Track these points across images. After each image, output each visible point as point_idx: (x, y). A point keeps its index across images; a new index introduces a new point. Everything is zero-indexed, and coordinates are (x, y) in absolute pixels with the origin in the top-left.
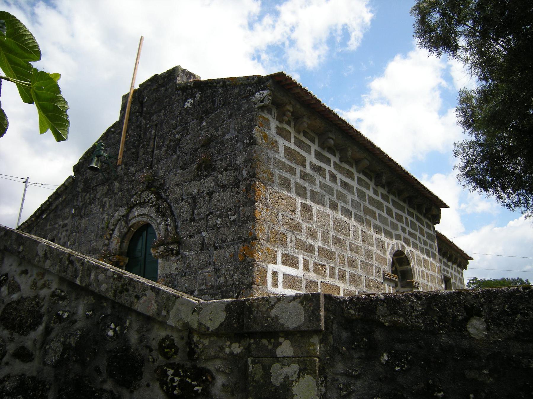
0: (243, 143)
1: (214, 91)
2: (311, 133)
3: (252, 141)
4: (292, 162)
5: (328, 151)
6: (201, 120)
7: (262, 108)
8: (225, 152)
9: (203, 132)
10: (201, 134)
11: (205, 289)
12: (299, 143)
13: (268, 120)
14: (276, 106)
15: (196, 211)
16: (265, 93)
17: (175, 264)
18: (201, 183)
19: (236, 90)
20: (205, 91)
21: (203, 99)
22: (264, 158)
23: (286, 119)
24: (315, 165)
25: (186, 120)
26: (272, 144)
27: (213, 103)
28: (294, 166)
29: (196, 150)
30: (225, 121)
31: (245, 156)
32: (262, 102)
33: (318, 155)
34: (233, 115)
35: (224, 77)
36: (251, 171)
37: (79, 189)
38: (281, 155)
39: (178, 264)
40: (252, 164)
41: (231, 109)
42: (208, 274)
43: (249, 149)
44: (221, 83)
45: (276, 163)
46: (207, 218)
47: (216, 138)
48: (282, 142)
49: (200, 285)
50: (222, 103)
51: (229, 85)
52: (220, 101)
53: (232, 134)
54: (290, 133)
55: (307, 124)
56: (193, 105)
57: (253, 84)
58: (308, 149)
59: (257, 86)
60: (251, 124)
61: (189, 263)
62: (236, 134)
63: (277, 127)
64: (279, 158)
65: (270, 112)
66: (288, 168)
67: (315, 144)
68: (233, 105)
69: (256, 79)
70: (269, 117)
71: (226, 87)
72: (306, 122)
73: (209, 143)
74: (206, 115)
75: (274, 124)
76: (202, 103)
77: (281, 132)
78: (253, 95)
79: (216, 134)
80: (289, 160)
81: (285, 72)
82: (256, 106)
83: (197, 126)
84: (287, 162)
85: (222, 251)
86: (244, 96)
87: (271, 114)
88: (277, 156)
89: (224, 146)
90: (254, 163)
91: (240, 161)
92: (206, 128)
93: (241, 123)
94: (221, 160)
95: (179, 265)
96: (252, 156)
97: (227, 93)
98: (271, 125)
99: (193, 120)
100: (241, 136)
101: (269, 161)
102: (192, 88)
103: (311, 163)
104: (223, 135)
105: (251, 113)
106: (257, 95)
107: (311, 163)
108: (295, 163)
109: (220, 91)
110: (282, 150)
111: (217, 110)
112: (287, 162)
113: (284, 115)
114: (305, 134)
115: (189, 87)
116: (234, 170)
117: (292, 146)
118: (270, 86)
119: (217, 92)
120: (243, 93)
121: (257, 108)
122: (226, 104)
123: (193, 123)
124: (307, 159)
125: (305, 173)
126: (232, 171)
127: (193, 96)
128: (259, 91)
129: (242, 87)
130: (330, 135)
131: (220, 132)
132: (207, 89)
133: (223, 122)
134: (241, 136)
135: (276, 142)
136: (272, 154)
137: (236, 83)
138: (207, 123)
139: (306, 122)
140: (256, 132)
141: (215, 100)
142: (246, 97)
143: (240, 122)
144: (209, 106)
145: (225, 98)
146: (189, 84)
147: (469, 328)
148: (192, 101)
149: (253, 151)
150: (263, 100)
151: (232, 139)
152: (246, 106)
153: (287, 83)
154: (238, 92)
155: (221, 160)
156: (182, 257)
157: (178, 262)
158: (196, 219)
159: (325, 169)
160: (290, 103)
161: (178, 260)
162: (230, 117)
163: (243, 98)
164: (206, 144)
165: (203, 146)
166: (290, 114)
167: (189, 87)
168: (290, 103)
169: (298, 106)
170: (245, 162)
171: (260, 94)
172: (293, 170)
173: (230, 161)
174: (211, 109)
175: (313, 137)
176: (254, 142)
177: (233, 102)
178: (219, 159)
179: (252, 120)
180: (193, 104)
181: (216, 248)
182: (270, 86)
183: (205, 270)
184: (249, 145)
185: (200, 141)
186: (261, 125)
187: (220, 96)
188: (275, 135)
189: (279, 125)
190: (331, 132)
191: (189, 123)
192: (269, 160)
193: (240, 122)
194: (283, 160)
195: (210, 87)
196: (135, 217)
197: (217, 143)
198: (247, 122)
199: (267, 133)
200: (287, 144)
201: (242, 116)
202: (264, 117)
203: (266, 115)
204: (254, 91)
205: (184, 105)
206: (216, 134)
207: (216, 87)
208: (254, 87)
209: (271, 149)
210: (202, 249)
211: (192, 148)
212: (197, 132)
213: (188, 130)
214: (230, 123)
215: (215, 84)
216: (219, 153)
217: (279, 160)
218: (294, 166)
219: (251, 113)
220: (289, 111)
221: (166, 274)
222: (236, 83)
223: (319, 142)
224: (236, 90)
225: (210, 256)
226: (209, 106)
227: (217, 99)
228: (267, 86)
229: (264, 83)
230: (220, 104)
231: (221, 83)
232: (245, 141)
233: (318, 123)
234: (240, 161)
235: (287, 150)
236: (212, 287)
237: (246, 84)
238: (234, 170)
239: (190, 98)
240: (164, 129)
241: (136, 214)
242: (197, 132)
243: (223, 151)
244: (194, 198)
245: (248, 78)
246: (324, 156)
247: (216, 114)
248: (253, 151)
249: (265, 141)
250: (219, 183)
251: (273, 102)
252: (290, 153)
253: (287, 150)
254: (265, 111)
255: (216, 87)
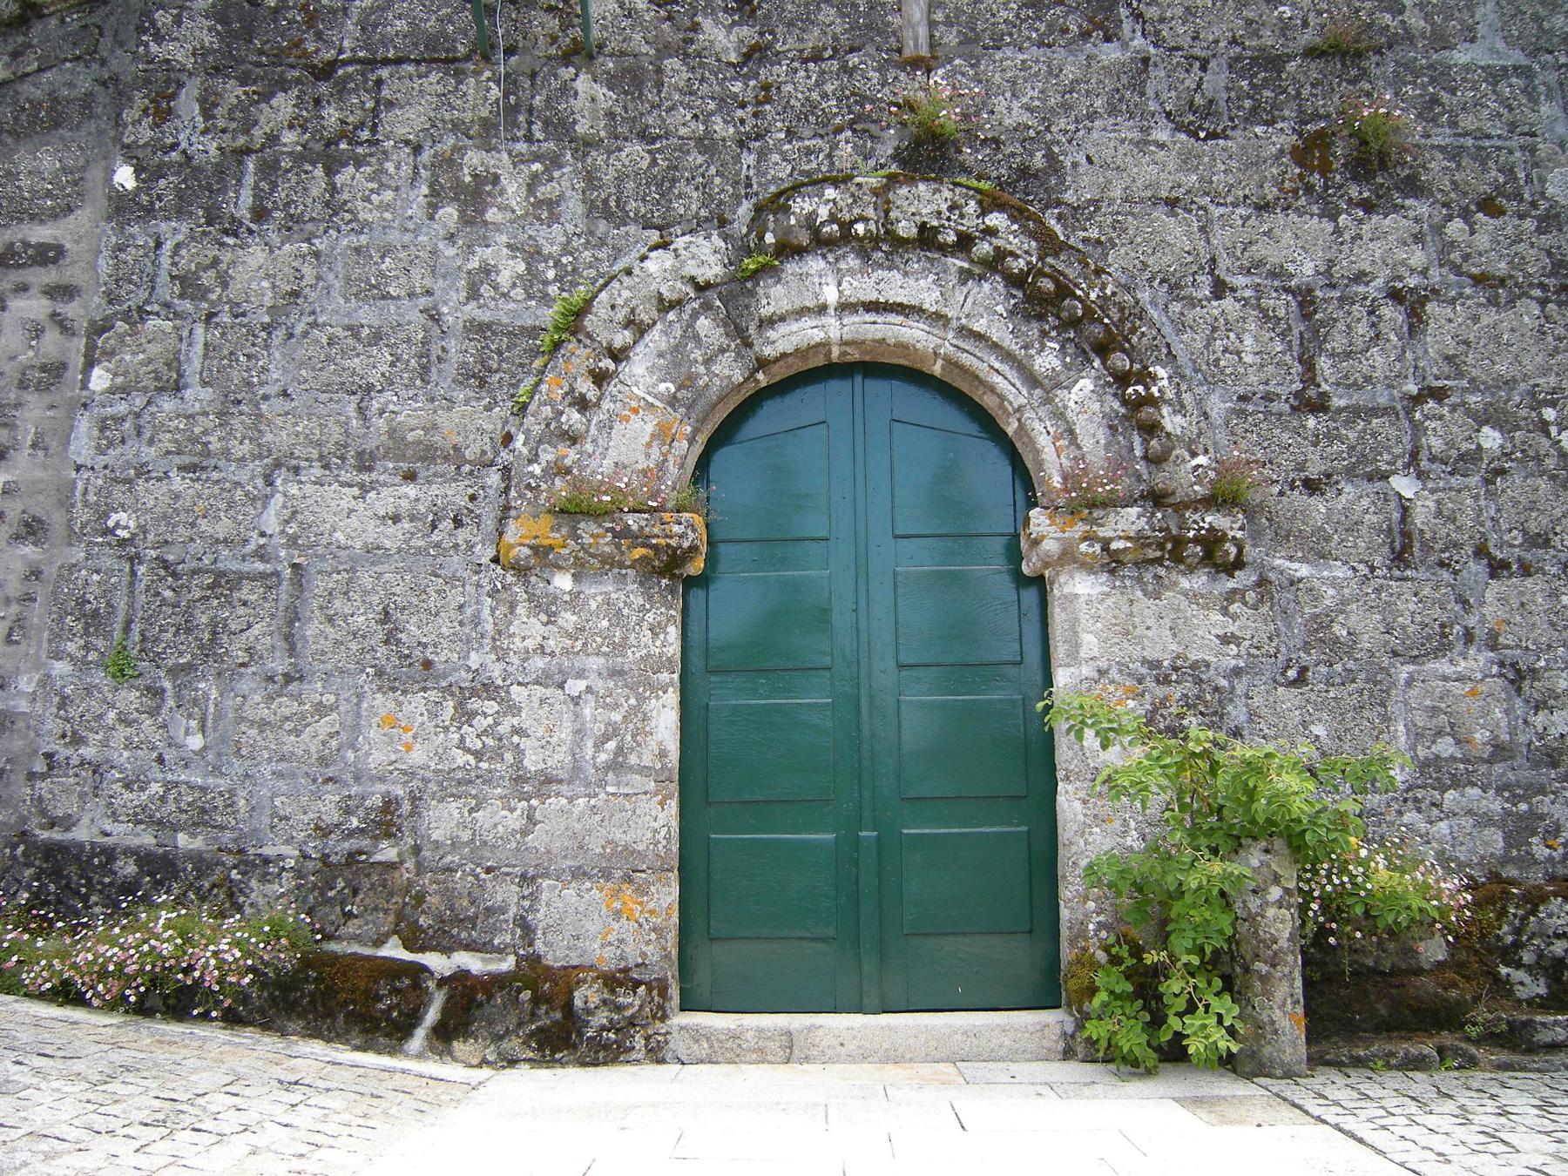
11: (1453, 758)
15: (1323, 363)
17: (1216, 617)
18: (1338, 231)
37: (178, 53)
39: (1234, 617)
42: (1458, 689)
46: (1409, 413)
49: (1416, 735)
61: (1320, 624)
85: (1534, 586)
95: (1247, 622)
116: (1540, 219)
126: (1529, 224)
147: (619, 870)
156: (1262, 582)
157: (1235, 607)
158: (1337, 402)
161: (1231, 595)
181: (1497, 568)
183: (1443, 666)
196: (822, 309)
210: (1400, 557)
221: (1155, 665)
225: (1464, 602)
236: (1500, 751)
238: (1540, 219)
240: (658, 698)
241: (831, 295)
244: (1305, 300)
250: (1455, 256)
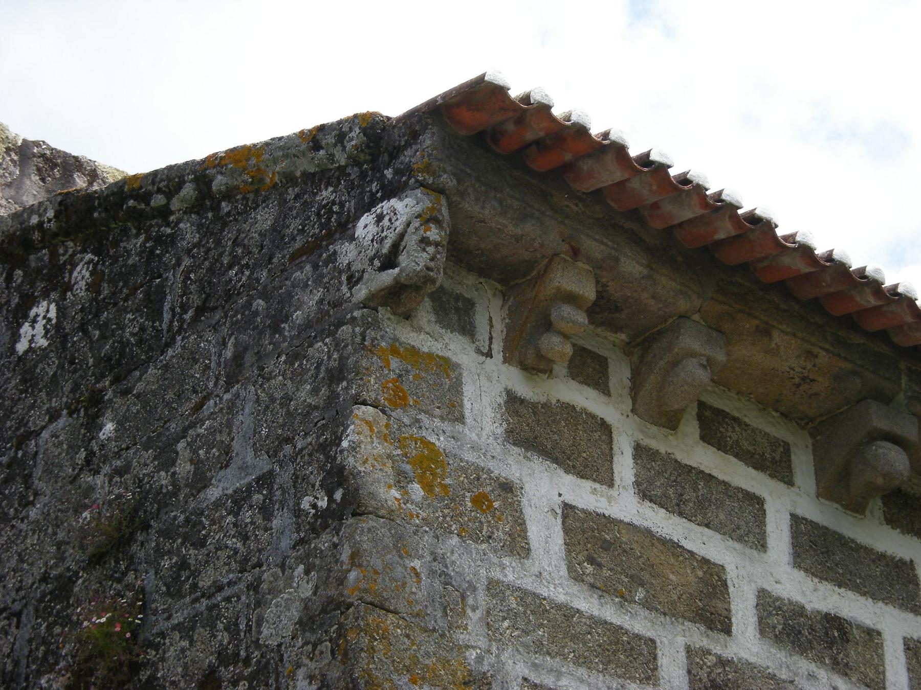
0: (298, 512)
1: (159, 240)
2: (755, 420)
3: (338, 495)
4: (625, 599)
5: (891, 521)
6: (94, 407)
7: (398, 298)
8: (205, 582)
9: (99, 480)
10: (91, 489)
12: (666, 483)
13: (446, 366)
14: (482, 273)
16: (403, 208)
19: (264, 218)
20: (116, 244)
21: (106, 290)
22: (422, 591)
23: (556, 346)
24: (799, 611)
25: (22, 423)
26: (480, 501)
27: (153, 304)
28: (637, 623)
29: (63, 588)
30: (206, 398)
31: (307, 590)
32: (389, 262)
33: (818, 550)
34: (249, 358)
35: (199, 153)
36: (334, 674)
38: (546, 568)
40: (342, 632)
41: (236, 328)
43: (324, 542)
44: (188, 190)
45: (511, 614)
47: (164, 500)
48: (545, 489)
50: (196, 300)
51: (228, 195)
52: (186, 292)
53: (244, 468)
54: (605, 428)
55: (709, 363)
56: (57, 332)
57: (342, 169)
58: (744, 521)
59: (363, 175)
60: (333, 397)
62: (264, 464)
63: (513, 401)
64: (528, 584)
65: (457, 315)
66: (598, 638)
67: (790, 483)
68: (249, 304)
69: (355, 137)
70: (456, 348)
71: (216, 208)
72: (696, 359)
73: (129, 540)
74: (116, 380)
75: (486, 385)
76: (97, 315)
77: (536, 430)
78: (344, 228)
79: (163, 478)
80: (601, 589)
81: (498, 74)
82: (361, 292)
83: (73, 449)
84: (587, 604)
86: (297, 245)
87: (467, 330)
88: (511, 572)
89: (201, 544)
90: (349, 622)
91: (279, 621)
92: (117, 455)
93: (287, 398)
94: (186, 630)
96: (341, 581)
97: (218, 242)
98: (469, 390)
99: (54, 416)
100: (284, 477)
101: (453, 597)
102: (50, 239)
103: (767, 604)
104: (200, 482)
105: (332, 334)
106: (365, 227)
107: (767, 604)
108: (646, 605)
109: (188, 231)
110: (546, 537)
111: (170, 343)
112: (587, 604)
113: (547, 325)
114: (714, 428)
115: (36, 236)
116: (251, 678)
117: (623, 504)
118: (427, 169)
119: (173, 239)
120: (294, 225)
121: (364, 305)
122: (212, 302)
123: (53, 436)
124: (731, 574)
125: (723, 662)
127: (56, 281)
128: (374, 202)
129: (291, 193)
130: (879, 419)
131: (184, 468)
132: (125, 231)
133: (199, 407)
134: (284, 477)
135: (507, 487)
136: (470, 562)
137: (258, 180)
138: (120, 423)
139: (696, 359)
140: (365, 443)
141: (161, 287)
142: (313, 248)
143: (278, 395)
144: (132, 325)
145: (211, 270)
146: (35, 220)
148: (53, 314)
149: (345, 554)
150: (396, 248)
151: (239, 500)
152: (311, 300)
153: (529, 136)
154: (274, 228)
155: (186, 630)
159: (872, 635)
160: (575, 253)
162: (234, 373)
163: (294, 256)
164: (114, 548)
165: (97, 560)
166: (581, 318)
167: (36, 236)
168: (575, 253)
169: (632, 266)
170: (306, 623)
171: (380, 218)
172: (630, 651)
173: (232, 628)
174: (140, 342)
175: (775, 443)
176: (349, 503)
177: (249, 286)
178: (178, 627)
179: (337, 375)
180: (58, 326)
182: (427, 169)
184: (329, 519)
185: (84, 533)
186: (399, 400)
187: (187, 262)
188: (497, 449)
189: (524, 390)
190: (885, 399)
191: (38, 434)
192: (453, 597)
193: (278, 395)
194: (561, 589)
195: (138, 217)
197: (167, 533)
198: (315, 391)
199: (441, 443)
200: (585, 495)
201: (290, 362)
202: (414, 352)
203: (428, 337)
204: (350, 205)
205: (15, 337)
206: (163, 478)
207: (164, 213)
208: (351, 186)
209: (469, 534)
211: (45, 579)
212: (74, 479)
213: (27, 479)
214: (232, 408)
215: (158, 200)
216: (174, 591)
217: (524, 595)
218: (637, 623)
219: (332, 334)
220: (572, 299)
222: (258, 180)
223: (819, 471)
224: (264, 218)
226: (132, 325)
227: (174, 279)
228: (409, 170)
229: (395, 152)
230: (184, 308)
231: (188, 190)
232: (305, 504)
233: (785, 353)
234: (279, 621)
235: (587, 536)
237: (308, 177)
239: (45, 295)
242: (74, 479)
243: (195, 574)
245: (315, 138)
246: (868, 551)
247: (166, 367)
248: (345, 554)
249: (428, 487)
251: (459, 252)
252: (606, 546)
253: (587, 536)
254: (425, 315)
255: (164, 213)
